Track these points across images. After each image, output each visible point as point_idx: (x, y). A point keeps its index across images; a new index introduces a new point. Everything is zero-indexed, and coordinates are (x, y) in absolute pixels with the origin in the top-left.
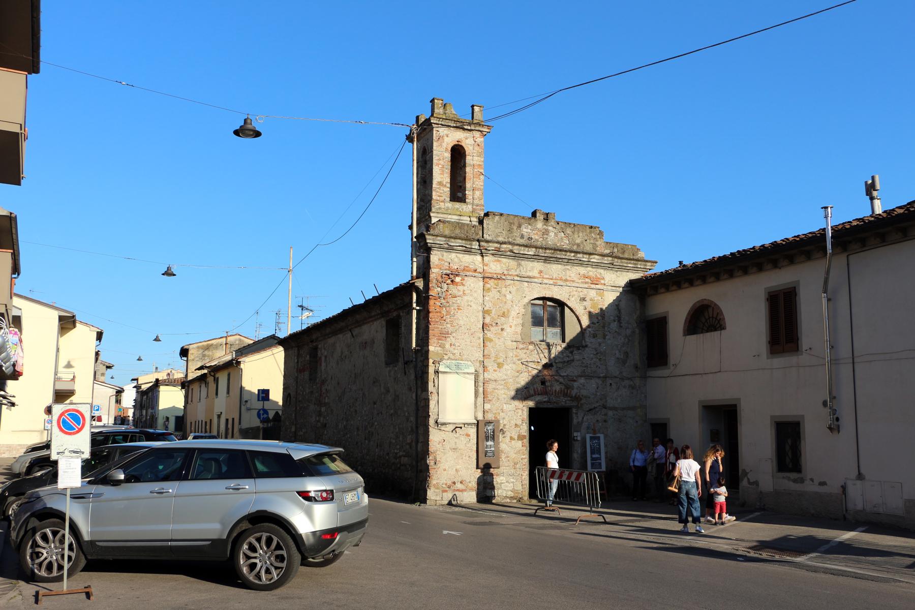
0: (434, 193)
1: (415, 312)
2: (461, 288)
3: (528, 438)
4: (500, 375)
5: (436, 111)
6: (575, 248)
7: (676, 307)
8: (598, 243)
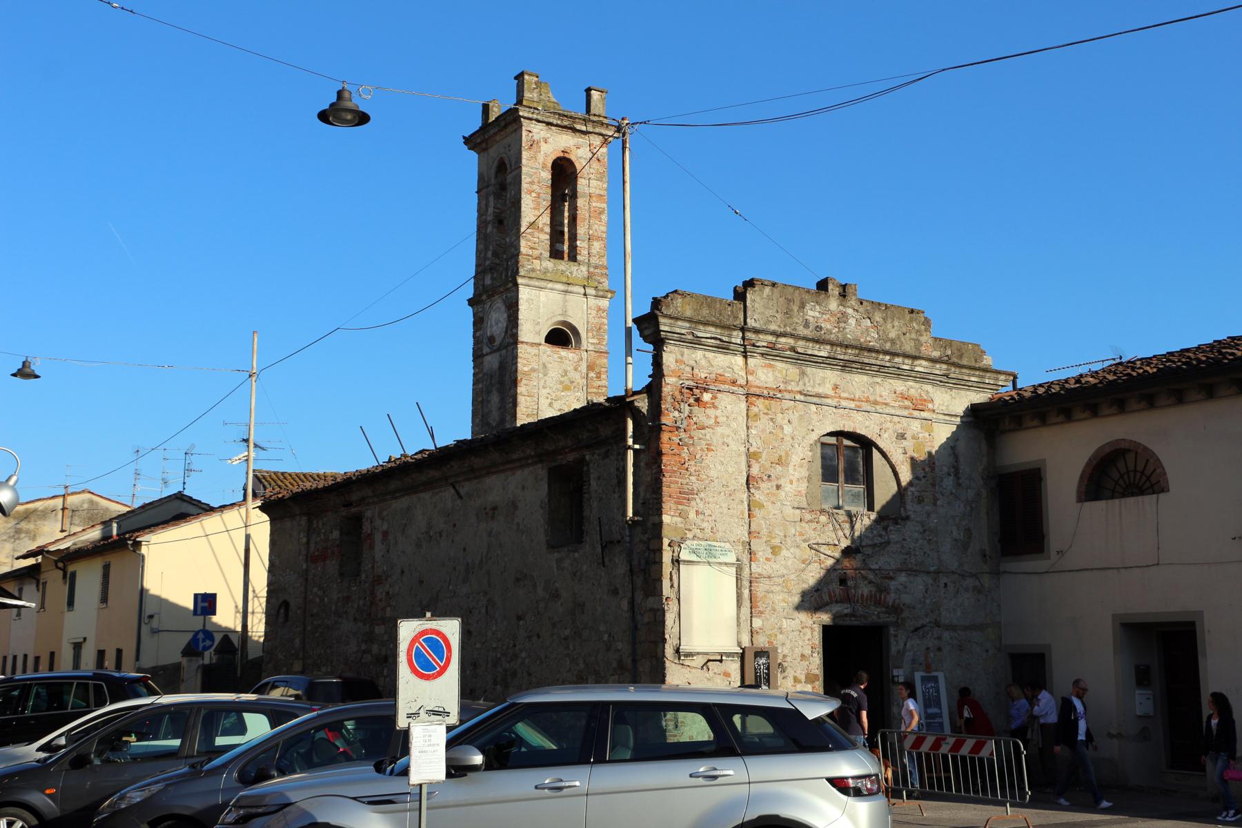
0: (523, 243)
1: (630, 454)
2: (711, 412)
3: (821, 679)
4: (776, 566)
5: (527, 95)
6: (888, 346)
7: (1063, 454)
8: (923, 339)
